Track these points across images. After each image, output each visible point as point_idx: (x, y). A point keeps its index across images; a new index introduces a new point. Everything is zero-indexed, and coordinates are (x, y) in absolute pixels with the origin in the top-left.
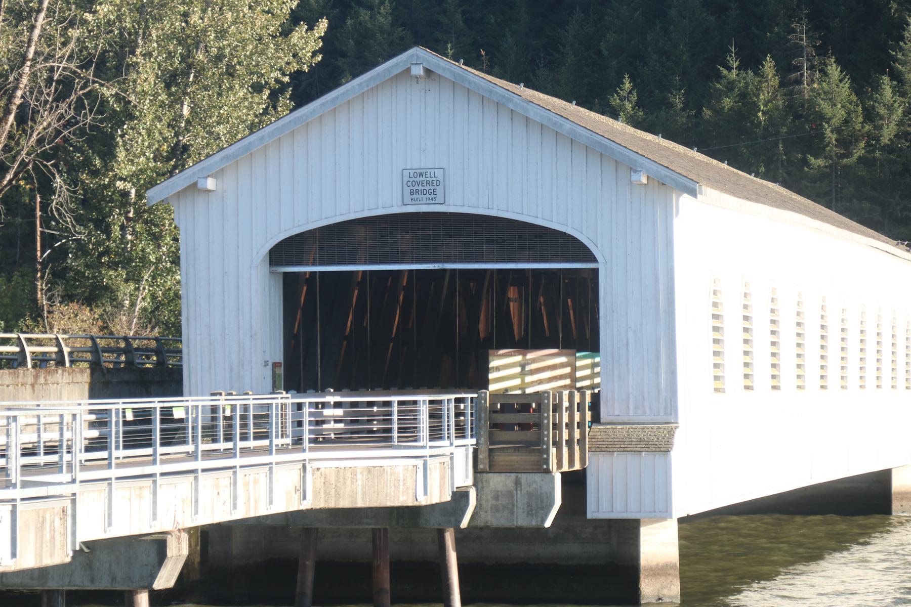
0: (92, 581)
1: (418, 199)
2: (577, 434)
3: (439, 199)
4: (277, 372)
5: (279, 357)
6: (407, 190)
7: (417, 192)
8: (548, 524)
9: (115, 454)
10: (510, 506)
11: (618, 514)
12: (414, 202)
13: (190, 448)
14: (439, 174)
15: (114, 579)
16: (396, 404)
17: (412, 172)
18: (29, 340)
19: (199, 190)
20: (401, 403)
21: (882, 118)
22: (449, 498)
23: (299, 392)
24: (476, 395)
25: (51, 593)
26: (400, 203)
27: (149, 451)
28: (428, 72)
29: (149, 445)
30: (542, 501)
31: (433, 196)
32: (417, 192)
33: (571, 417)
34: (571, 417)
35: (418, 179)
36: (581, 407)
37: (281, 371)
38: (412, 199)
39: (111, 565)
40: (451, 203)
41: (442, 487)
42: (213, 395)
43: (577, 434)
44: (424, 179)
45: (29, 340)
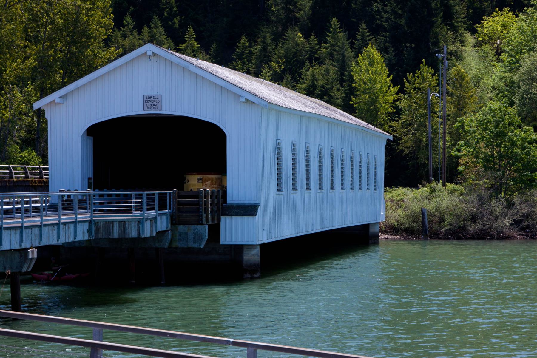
1: (150, 108)
3: (159, 108)
4: (90, 181)
5: (91, 176)
6: (145, 104)
7: (150, 105)
8: (202, 246)
10: (186, 239)
11: (234, 242)
12: (148, 109)
14: (159, 97)
17: (148, 96)
20: (148, 194)
23: (99, 190)
26: (142, 110)
28: (154, 54)
29: (57, 210)
30: (200, 237)
31: (156, 107)
32: (150, 105)
35: (150, 99)
37: (92, 181)
39: (4, 262)
40: (164, 110)
41: (151, 231)
44: (153, 99)
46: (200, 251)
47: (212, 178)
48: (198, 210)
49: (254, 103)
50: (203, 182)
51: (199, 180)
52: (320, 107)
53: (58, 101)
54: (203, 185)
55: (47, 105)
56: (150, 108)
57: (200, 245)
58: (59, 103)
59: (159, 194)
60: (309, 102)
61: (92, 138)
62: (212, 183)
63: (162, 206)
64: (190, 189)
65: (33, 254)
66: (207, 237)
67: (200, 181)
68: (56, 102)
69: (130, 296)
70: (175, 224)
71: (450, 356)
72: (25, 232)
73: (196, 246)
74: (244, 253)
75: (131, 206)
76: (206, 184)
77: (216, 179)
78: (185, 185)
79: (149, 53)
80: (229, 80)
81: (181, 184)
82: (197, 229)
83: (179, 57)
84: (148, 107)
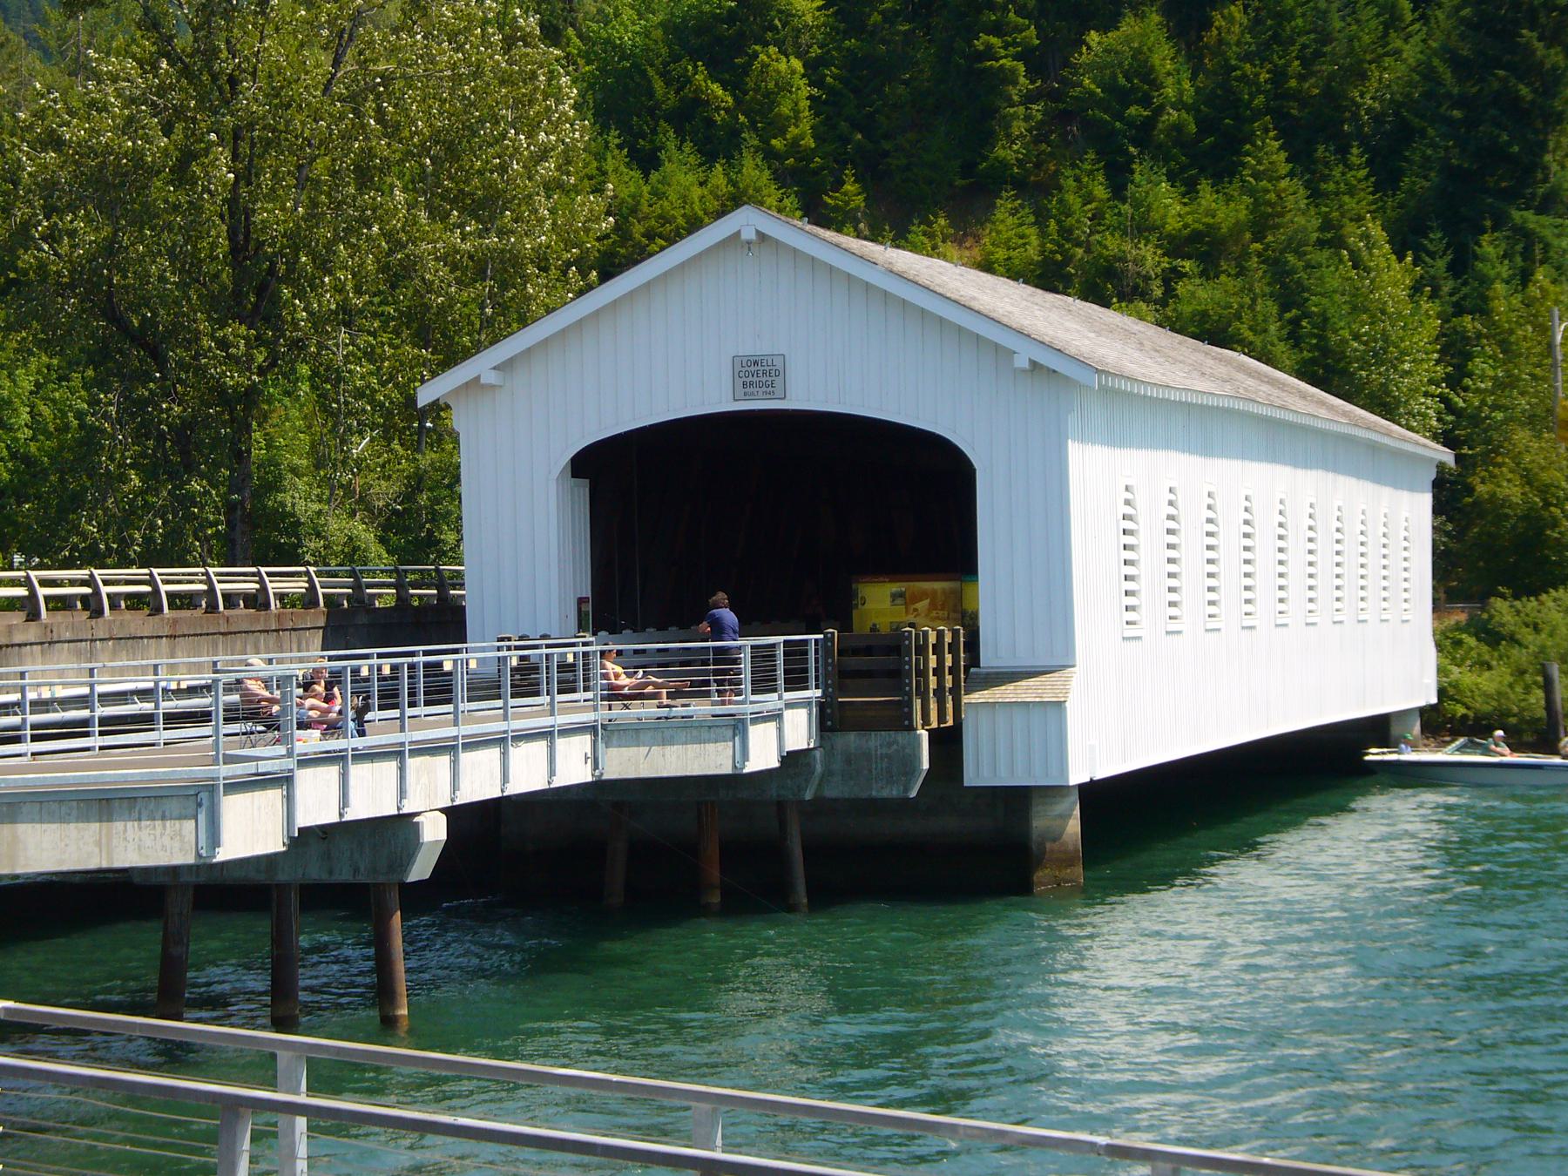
0: (331, 873)
1: (752, 394)
2: (949, 683)
3: (779, 392)
6: (739, 382)
7: (751, 384)
8: (913, 794)
9: (461, 707)
11: (1004, 779)
12: (747, 397)
13: (545, 699)
14: (778, 362)
15: (356, 871)
16: (749, 650)
17: (745, 360)
18: (45, 583)
19: (483, 387)
21: (102, 166)
22: (776, 764)
24: (821, 636)
25: (283, 888)
27: (499, 703)
28: (762, 237)
31: (770, 389)
32: (751, 384)
33: (941, 661)
34: (941, 661)
35: (753, 369)
36: (953, 648)
38: (745, 394)
42: (501, 640)
43: (949, 683)
45: (269, 574)
46: (903, 806)
47: (934, 592)
48: (899, 688)
49: (1054, 371)
50: (906, 604)
51: (894, 596)
52: (1240, 376)
53: (489, 378)
54: (907, 612)
55: (457, 391)
56: (752, 394)
57: (907, 790)
58: (492, 387)
59: (785, 641)
60: (1210, 362)
61: (587, 481)
62: (933, 606)
63: (796, 680)
64: (869, 625)
65: (434, 830)
66: (926, 765)
67: (899, 601)
68: (482, 381)
69: (618, 948)
70: (832, 730)
71: (609, 1172)
72: (412, 763)
73: (894, 793)
74: (1034, 809)
75: (707, 683)
76: (915, 610)
77: (944, 592)
78: (855, 613)
79: (748, 234)
80: (976, 305)
81: (839, 609)
82: (896, 742)
83: (837, 245)
84: (747, 390)
